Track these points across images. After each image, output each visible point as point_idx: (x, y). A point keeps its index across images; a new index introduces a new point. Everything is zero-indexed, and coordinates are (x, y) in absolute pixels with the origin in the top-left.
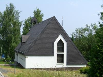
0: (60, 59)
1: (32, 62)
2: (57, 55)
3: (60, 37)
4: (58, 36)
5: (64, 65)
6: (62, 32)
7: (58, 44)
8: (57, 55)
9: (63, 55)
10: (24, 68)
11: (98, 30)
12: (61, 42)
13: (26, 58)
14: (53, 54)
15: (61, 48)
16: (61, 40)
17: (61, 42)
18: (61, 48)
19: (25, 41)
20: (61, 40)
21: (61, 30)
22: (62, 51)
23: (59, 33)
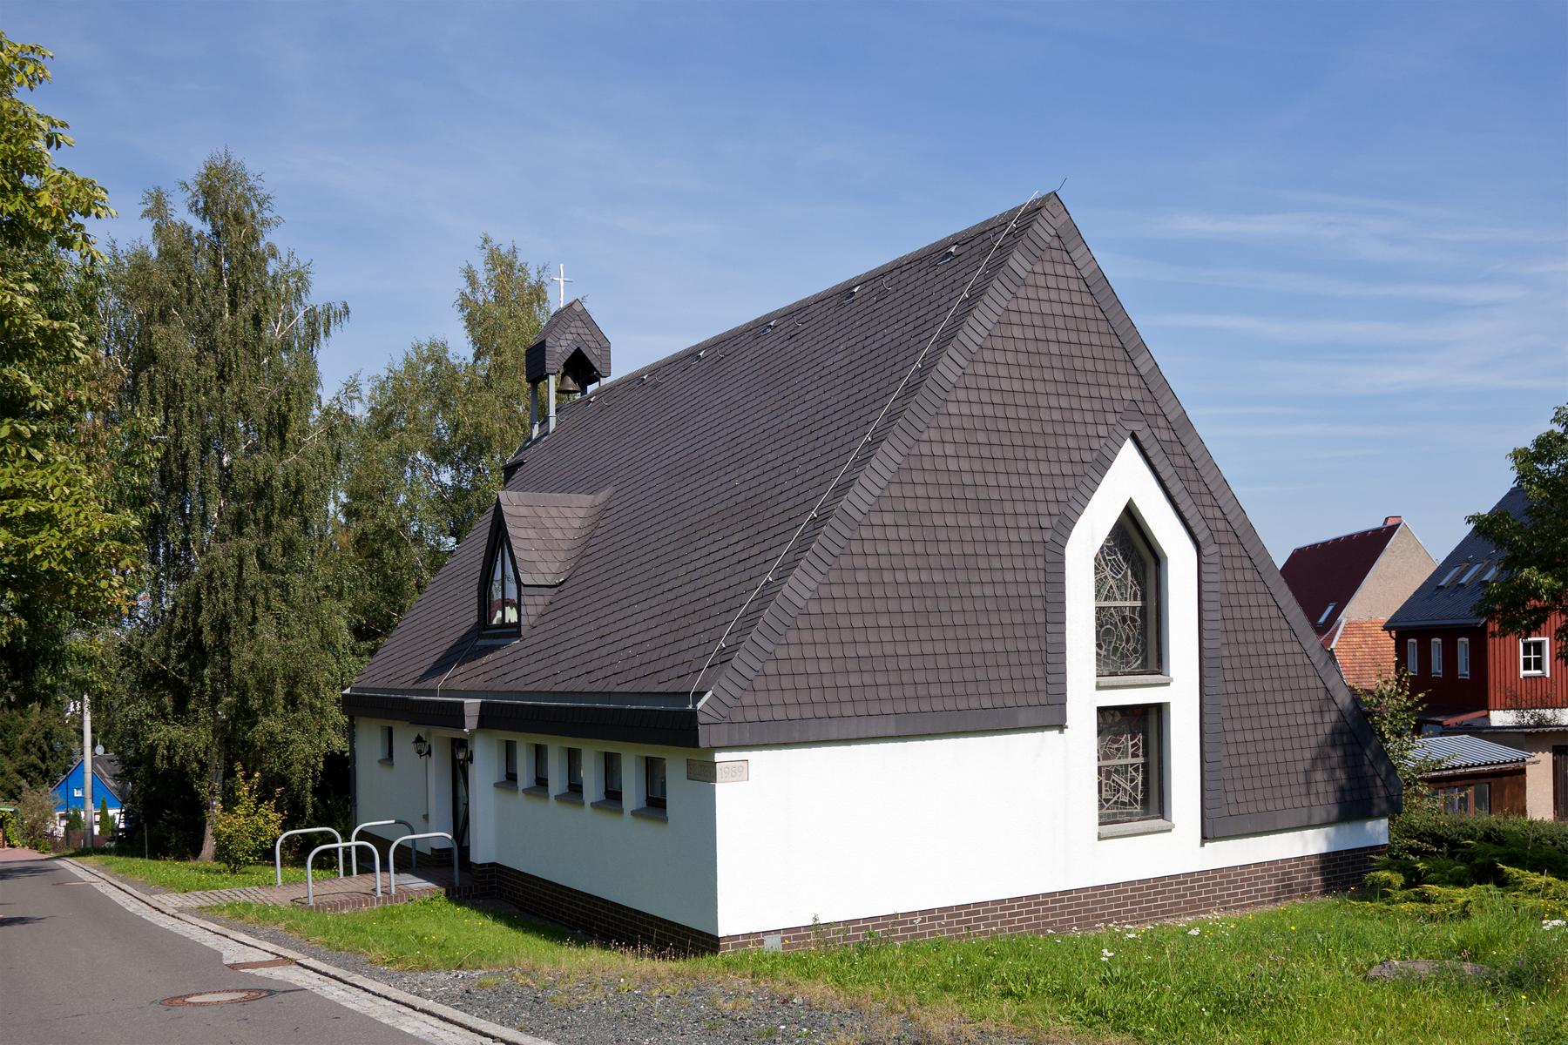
0: (1134, 793)
1: (814, 835)
2: (1102, 711)
3: (1128, 481)
4: (1102, 464)
5: (1177, 848)
6: (1150, 409)
7: (1102, 561)
8: (1102, 711)
9: (1157, 712)
10: (706, 943)
11: (264, 260)
12: (1131, 543)
13: (726, 793)
14: (1057, 722)
15: (1134, 640)
16: (1130, 512)
17: (1131, 543)
18: (1134, 640)
19: (555, 567)
20: (1130, 512)
21: (1134, 382)
22: (1152, 660)
23: (1111, 418)
